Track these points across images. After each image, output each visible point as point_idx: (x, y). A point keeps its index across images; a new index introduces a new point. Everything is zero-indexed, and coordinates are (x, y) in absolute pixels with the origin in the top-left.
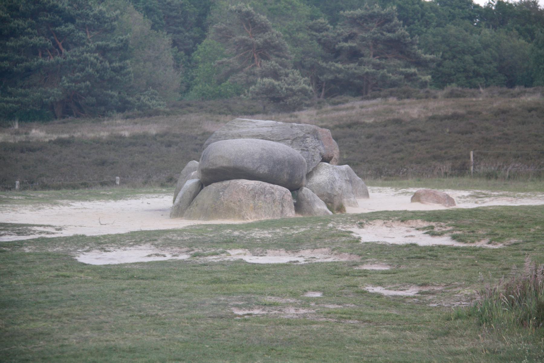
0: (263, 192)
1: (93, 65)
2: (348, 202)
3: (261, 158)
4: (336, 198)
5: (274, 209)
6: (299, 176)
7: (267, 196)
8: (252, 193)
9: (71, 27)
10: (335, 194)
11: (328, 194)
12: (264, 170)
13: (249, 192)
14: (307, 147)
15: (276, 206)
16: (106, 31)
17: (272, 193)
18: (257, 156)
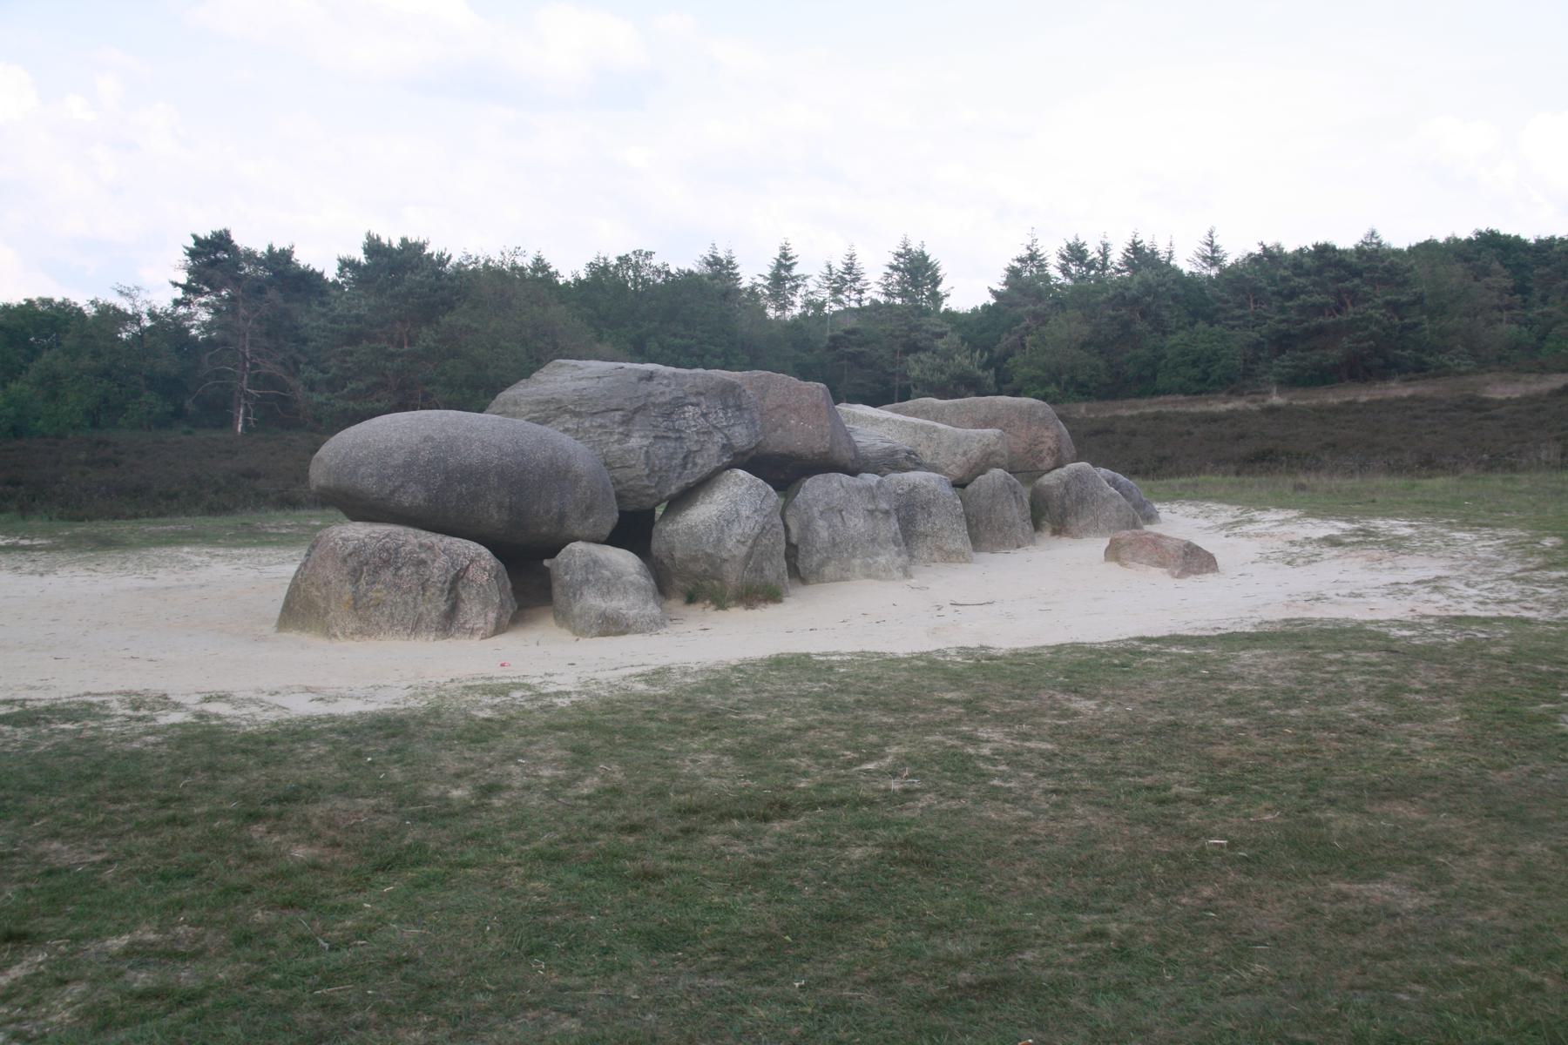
0: (388, 559)
1: (1378, 322)
2: (868, 566)
3: (408, 465)
4: (727, 567)
5: (421, 609)
6: (548, 512)
7: (404, 571)
8: (353, 562)
9: (1357, 281)
10: (725, 555)
11: (709, 555)
12: (412, 496)
13: (345, 561)
14: (678, 431)
15: (430, 601)
16: (1398, 284)
17: (423, 562)
18: (399, 458)
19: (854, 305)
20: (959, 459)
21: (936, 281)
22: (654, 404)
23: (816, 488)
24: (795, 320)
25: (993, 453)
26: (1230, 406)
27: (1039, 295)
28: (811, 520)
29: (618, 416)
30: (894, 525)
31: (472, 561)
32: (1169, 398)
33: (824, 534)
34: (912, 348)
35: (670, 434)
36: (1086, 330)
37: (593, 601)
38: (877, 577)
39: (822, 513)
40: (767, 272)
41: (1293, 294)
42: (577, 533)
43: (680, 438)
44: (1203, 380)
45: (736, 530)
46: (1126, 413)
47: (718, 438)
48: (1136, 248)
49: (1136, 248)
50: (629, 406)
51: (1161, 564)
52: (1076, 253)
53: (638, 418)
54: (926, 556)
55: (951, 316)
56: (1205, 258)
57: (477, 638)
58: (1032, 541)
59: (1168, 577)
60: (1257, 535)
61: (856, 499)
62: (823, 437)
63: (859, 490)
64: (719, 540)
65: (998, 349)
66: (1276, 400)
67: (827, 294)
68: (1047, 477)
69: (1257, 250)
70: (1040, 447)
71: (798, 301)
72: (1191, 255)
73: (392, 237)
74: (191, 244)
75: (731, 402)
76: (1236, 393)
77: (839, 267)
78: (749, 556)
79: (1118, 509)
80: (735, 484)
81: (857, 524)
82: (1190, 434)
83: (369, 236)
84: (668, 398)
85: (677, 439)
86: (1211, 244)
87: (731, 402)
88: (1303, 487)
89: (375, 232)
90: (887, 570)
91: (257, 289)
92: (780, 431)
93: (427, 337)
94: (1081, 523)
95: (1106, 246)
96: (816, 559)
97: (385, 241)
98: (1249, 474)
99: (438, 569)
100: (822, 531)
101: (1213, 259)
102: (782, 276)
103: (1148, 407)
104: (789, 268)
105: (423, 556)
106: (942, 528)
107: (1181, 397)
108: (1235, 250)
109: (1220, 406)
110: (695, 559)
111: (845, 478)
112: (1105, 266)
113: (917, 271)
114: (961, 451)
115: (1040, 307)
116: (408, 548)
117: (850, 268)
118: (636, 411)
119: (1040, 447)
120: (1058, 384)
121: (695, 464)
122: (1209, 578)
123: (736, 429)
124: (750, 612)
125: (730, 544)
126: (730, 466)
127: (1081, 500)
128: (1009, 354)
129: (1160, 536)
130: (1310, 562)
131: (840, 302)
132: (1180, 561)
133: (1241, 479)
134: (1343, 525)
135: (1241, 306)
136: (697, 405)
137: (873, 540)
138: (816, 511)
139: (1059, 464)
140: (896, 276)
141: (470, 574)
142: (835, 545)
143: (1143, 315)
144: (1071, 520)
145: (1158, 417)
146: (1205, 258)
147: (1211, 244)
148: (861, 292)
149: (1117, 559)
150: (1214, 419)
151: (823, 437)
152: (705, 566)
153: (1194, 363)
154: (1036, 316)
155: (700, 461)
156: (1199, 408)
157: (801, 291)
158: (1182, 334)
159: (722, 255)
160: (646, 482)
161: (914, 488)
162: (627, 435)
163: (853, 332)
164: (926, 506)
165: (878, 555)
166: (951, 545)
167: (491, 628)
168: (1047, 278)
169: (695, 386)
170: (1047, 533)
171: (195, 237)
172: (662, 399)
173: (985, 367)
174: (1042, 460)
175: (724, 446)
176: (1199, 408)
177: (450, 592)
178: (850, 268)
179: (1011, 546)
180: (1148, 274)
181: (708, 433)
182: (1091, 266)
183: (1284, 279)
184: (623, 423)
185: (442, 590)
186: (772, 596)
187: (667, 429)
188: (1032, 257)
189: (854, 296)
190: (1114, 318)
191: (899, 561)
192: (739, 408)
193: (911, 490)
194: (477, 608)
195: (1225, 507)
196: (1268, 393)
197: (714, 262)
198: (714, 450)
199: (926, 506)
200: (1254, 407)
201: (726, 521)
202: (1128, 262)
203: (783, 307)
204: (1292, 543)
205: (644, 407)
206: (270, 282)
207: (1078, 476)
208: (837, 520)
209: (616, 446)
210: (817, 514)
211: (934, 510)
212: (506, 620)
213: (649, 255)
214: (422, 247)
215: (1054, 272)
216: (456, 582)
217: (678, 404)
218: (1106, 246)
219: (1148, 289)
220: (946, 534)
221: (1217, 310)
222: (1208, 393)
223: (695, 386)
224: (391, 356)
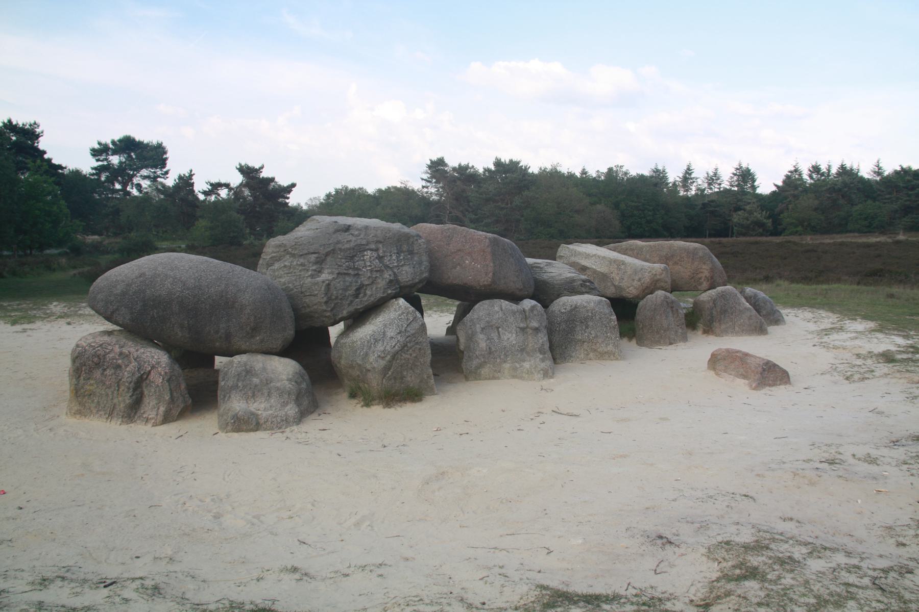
2: (515, 369)
3: (124, 294)
5: (116, 401)
6: (217, 332)
10: (369, 367)
11: (360, 365)
14: (358, 269)
17: (119, 367)
18: (119, 289)
19: (716, 190)
20: (636, 283)
21: (754, 180)
22: (340, 249)
23: (482, 309)
24: (693, 196)
25: (658, 280)
26: (878, 240)
27: (796, 187)
28: (474, 334)
29: (313, 257)
30: (543, 338)
31: (153, 367)
32: (852, 234)
33: (483, 345)
34: (738, 209)
35: (351, 271)
36: (816, 202)
37: (237, 405)
38: (522, 378)
39: (483, 329)
40: (681, 175)
41: (913, 189)
42: (243, 347)
43: (358, 274)
44: (868, 227)
45: (380, 347)
46: (828, 241)
47: (387, 275)
48: (843, 167)
49: (843, 167)
50: (323, 251)
51: (744, 377)
52: (816, 169)
53: (329, 259)
54: (582, 356)
55: (760, 197)
56: (875, 172)
57: (150, 425)
58: (685, 339)
59: (747, 388)
60: (835, 348)
61: (511, 319)
62: (486, 274)
63: (514, 313)
64: (367, 354)
65: (777, 210)
66: (901, 237)
67: (706, 185)
68: (704, 295)
69: (899, 169)
70: (700, 276)
71: (694, 188)
72: (869, 171)
73: (505, 158)
74: (429, 163)
75: (405, 248)
76: (883, 233)
77: (711, 174)
78: (387, 368)
79: (750, 318)
80: (395, 310)
81: (510, 337)
82: (854, 253)
83: (497, 159)
84: (352, 244)
85: (355, 275)
86: (878, 166)
87: (405, 248)
88: (891, 296)
89: (499, 157)
90: (529, 372)
91: (454, 180)
92: (458, 268)
93: (517, 201)
94: (723, 327)
95: (829, 166)
96: (475, 362)
97: (503, 160)
98: (865, 284)
99: (128, 373)
100: (482, 342)
101: (879, 173)
102: (687, 177)
103: (839, 238)
104: (690, 174)
105: (120, 361)
106: (596, 336)
107: (856, 234)
108: (889, 169)
109: (873, 239)
110: (352, 367)
111: (505, 304)
112: (829, 175)
113: (745, 176)
114: (637, 278)
115: (796, 192)
116: (111, 355)
117: (715, 174)
118: (327, 254)
119: (700, 276)
120: (803, 226)
121: (365, 295)
122: (780, 392)
123: (405, 268)
124: (387, 410)
125: (372, 358)
126: (396, 296)
127: (724, 312)
128: (781, 212)
129: (746, 355)
130: (864, 379)
131: (711, 189)
132: (758, 376)
133: (859, 287)
134: (900, 341)
135: (889, 193)
136: (377, 250)
137: (522, 350)
138: (478, 328)
139: (712, 287)
140: (735, 178)
141: (151, 377)
142: (490, 353)
143: (843, 197)
144: (716, 324)
145: (842, 244)
146: (875, 172)
147: (878, 166)
148: (720, 184)
149: (714, 369)
150: (868, 246)
151: (486, 274)
152: (358, 373)
153: (866, 219)
154: (795, 196)
155: (368, 292)
156: (864, 240)
157: (695, 184)
158: (860, 206)
159: (660, 168)
160: (324, 307)
161: (575, 308)
162: (320, 272)
163: (713, 201)
164: (585, 321)
165: (524, 361)
166: (602, 348)
167: (160, 418)
168: (801, 179)
169: (376, 236)
170: (700, 332)
171: (776, 185)
172: (347, 246)
173: (768, 218)
174: (701, 284)
175: (391, 281)
176: (864, 240)
177: (135, 390)
178: (715, 174)
179: (665, 344)
180: (847, 179)
181: (380, 271)
182: (822, 174)
183: (909, 181)
184: (316, 263)
185: (129, 388)
186: (413, 395)
187: (349, 268)
188: (796, 171)
189: (717, 186)
190: (829, 198)
191: (543, 365)
192: (411, 252)
193: (572, 310)
194: (153, 402)
195: (831, 314)
196: (898, 234)
197: (657, 171)
198: (382, 283)
199: (585, 321)
200: (890, 240)
201: (376, 339)
202: (839, 174)
203: (687, 191)
204: (858, 356)
205: (333, 251)
206: (459, 179)
207: (723, 296)
208: (494, 335)
209: (309, 279)
210: (478, 330)
211: (590, 324)
212: (175, 412)
213: (621, 167)
214: (518, 163)
215: (805, 177)
216: (139, 384)
217: (360, 249)
218: (829, 166)
219: (845, 184)
220: (600, 340)
221: (879, 195)
222: (870, 232)
223: (376, 236)
224: (502, 209)
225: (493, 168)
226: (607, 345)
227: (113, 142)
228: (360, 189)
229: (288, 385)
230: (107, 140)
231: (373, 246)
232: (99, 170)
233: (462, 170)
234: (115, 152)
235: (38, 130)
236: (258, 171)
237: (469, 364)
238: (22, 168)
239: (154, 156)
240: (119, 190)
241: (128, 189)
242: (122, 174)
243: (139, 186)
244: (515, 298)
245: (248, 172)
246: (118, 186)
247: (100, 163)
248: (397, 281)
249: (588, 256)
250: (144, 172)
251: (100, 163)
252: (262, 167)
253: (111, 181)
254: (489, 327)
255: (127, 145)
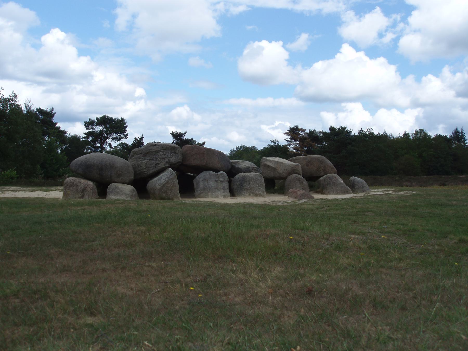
17: (78, 186)
25: (294, 170)
33: (201, 186)
100: (201, 185)
111: (211, 172)
193: (243, 177)
198: (164, 162)
208: (206, 183)
225: (328, 131)
226: (259, 191)
227: (97, 119)
228: (252, 147)
229: (128, 192)
230: (94, 117)
231: (162, 151)
232: (88, 134)
233: (312, 133)
234: (98, 124)
235: (54, 112)
236: (182, 135)
237: (196, 193)
238: (45, 134)
239: (118, 126)
240: (98, 147)
241: (104, 146)
242: (99, 138)
243: (110, 145)
244: (217, 171)
245: (177, 136)
246: (99, 145)
247: (89, 131)
248: (170, 162)
249: (270, 161)
250: (114, 135)
251: (89, 131)
252: (185, 133)
253: (94, 141)
254: (205, 180)
255: (104, 121)
